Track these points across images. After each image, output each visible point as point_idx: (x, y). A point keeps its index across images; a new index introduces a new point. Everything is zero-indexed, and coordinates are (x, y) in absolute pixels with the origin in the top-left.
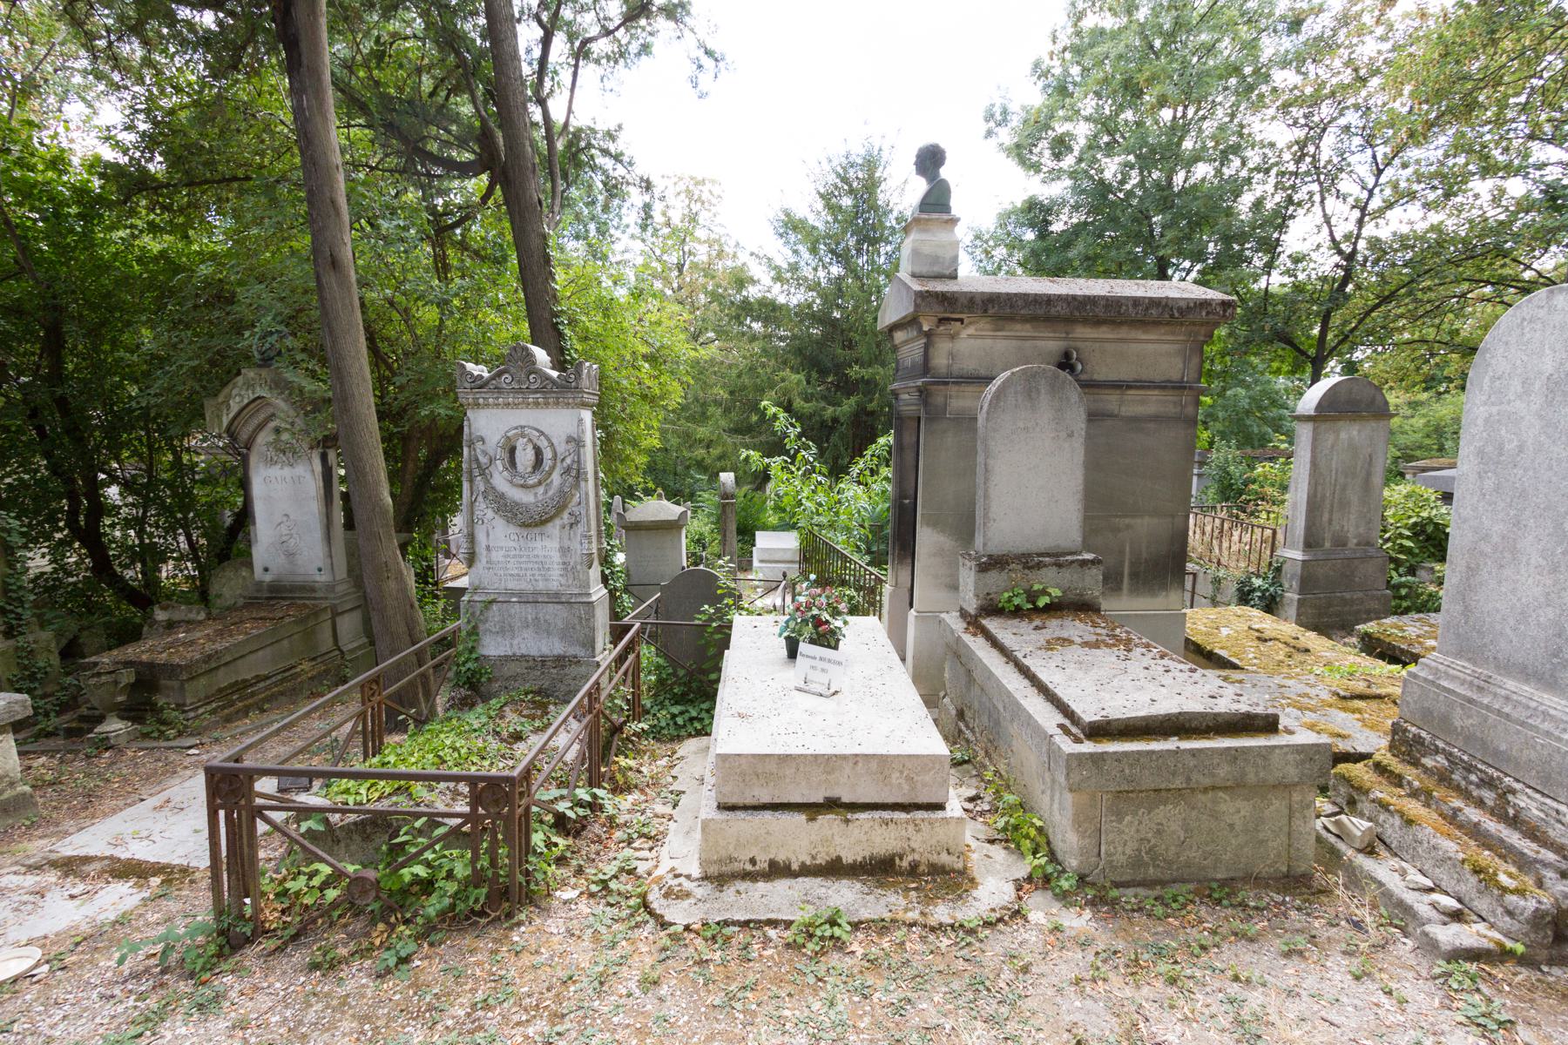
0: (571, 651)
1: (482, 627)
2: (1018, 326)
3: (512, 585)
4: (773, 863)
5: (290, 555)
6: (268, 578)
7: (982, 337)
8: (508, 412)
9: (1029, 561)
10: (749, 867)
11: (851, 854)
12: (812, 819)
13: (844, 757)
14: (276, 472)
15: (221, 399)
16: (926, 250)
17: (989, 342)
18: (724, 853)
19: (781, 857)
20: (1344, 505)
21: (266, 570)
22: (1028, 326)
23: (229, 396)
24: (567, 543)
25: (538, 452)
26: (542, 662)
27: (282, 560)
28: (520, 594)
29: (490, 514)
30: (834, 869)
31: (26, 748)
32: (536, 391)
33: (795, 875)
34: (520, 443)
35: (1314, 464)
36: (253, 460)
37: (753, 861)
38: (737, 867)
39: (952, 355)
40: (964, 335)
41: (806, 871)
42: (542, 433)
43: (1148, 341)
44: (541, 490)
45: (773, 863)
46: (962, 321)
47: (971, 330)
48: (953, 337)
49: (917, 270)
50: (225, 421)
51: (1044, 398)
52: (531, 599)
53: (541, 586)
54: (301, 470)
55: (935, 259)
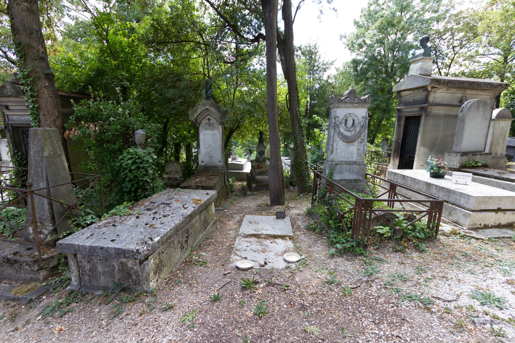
0: (359, 178)
1: (334, 171)
2: (453, 90)
3: (342, 159)
4: (485, 225)
5: (211, 157)
6: (203, 164)
7: (443, 92)
8: (346, 109)
9: (474, 153)
10: (479, 226)
11: (503, 223)
12: (497, 213)
13: (504, 197)
14: (207, 132)
15: (194, 109)
16: (424, 67)
17: (444, 94)
18: (474, 223)
19: (487, 224)
20: (498, 144)
21: (203, 162)
22: (455, 90)
23: (198, 108)
24: (359, 147)
26: (351, 181)
27: (208, 158)
28: (345, 162)
29: (338, 139)
30: (499, 226)
31: (217, 209)
32: (357, 103)
33: (490, 228)
35: (493, 133)
36: (200, 128)
37: (480, 225)
38: (476, 226)
39: (434, 97)
40: (438, 92)
41: (493, 227)
43: (484, 95)
44: (353, 132)
45: (485, 225)
46: (437, 88)
47: (441, 91)
48: (435, 92)
49: (421, 73)
50: (195, 116)
51: (481, 109)
52: (349, 163)
53: (350, 160)
54: (215, 131)
55: (426, 70)
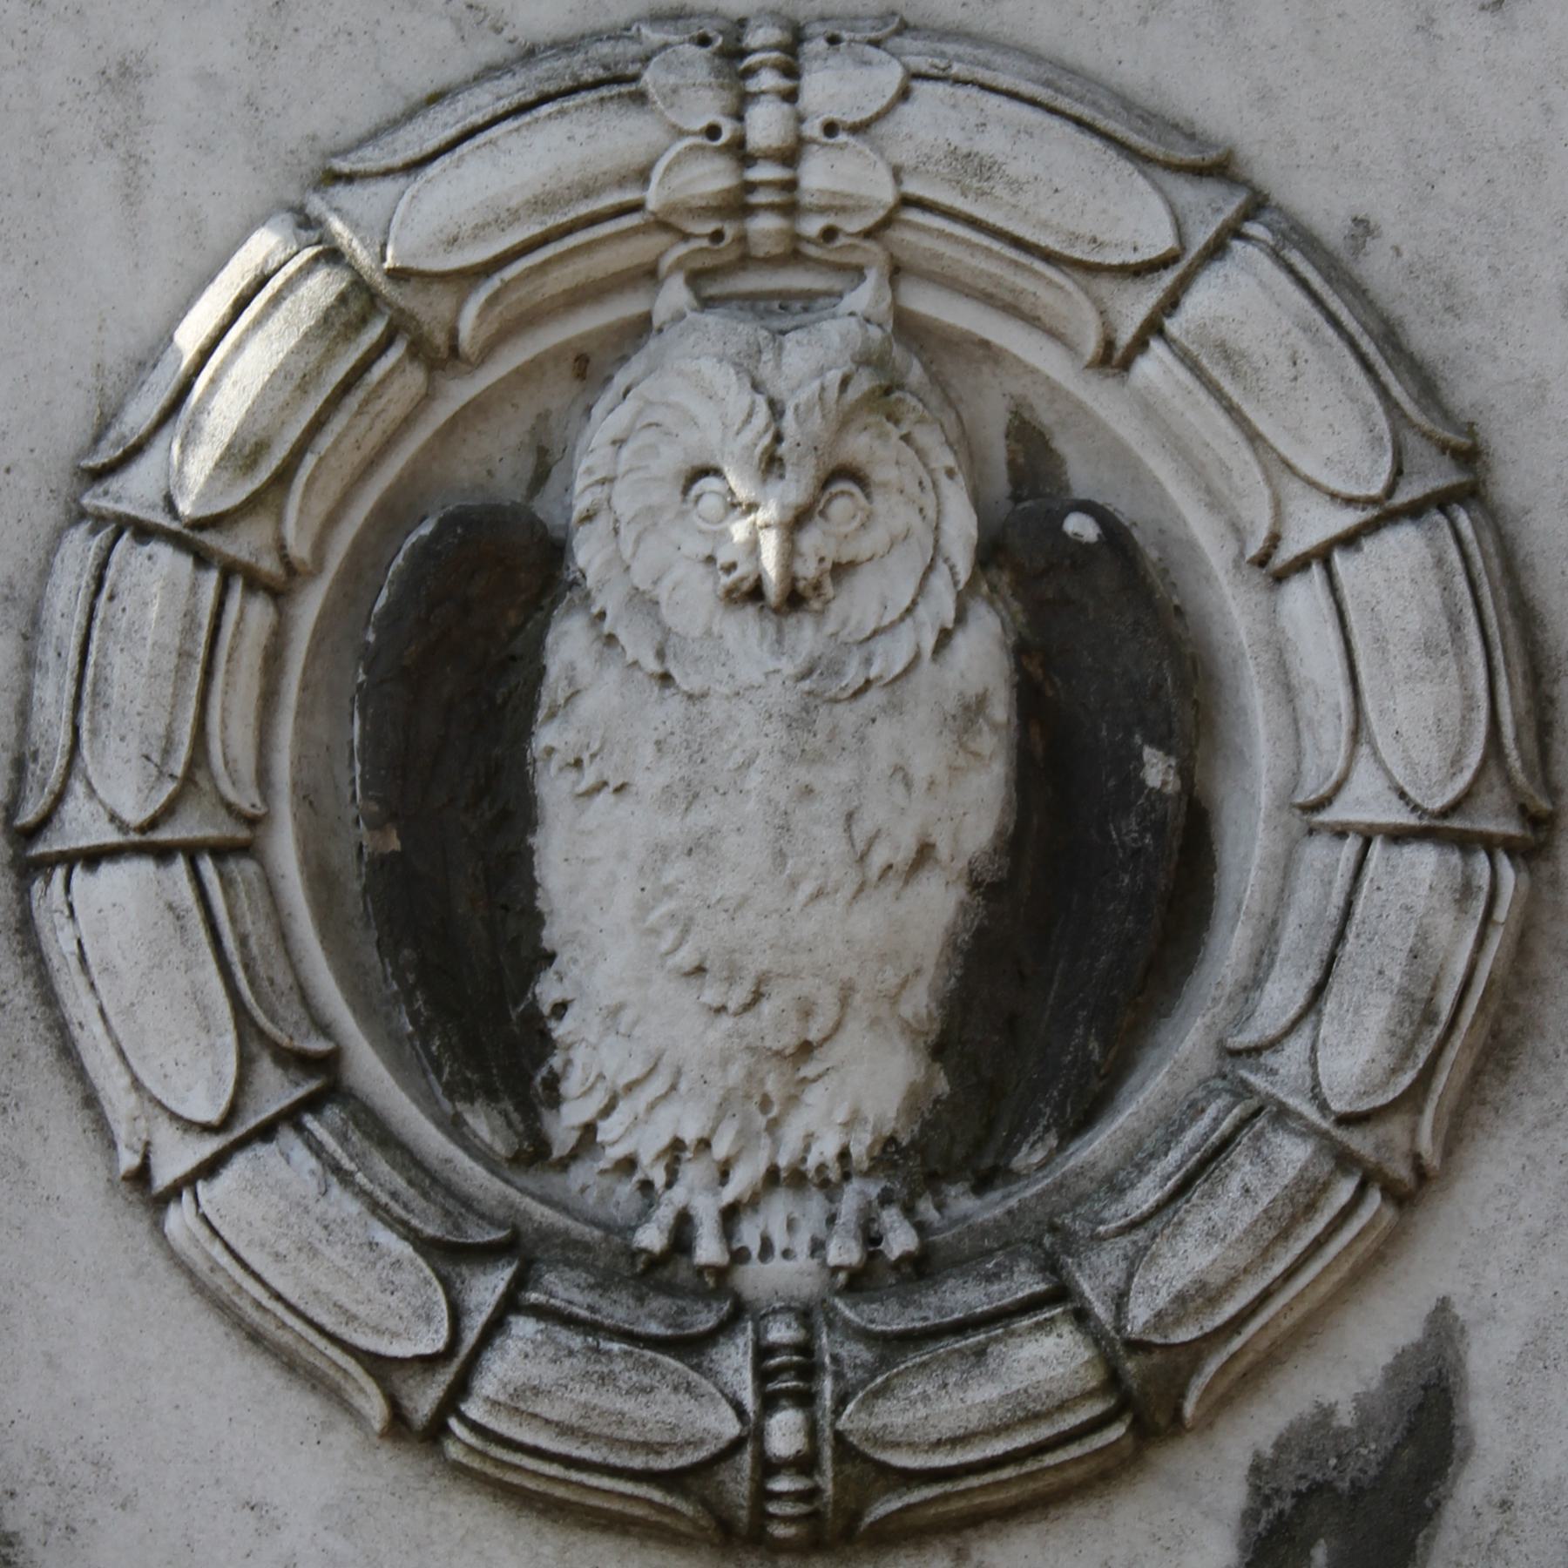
25: (1097, 658)
34: (680, 484)
42: (1450, 479)
